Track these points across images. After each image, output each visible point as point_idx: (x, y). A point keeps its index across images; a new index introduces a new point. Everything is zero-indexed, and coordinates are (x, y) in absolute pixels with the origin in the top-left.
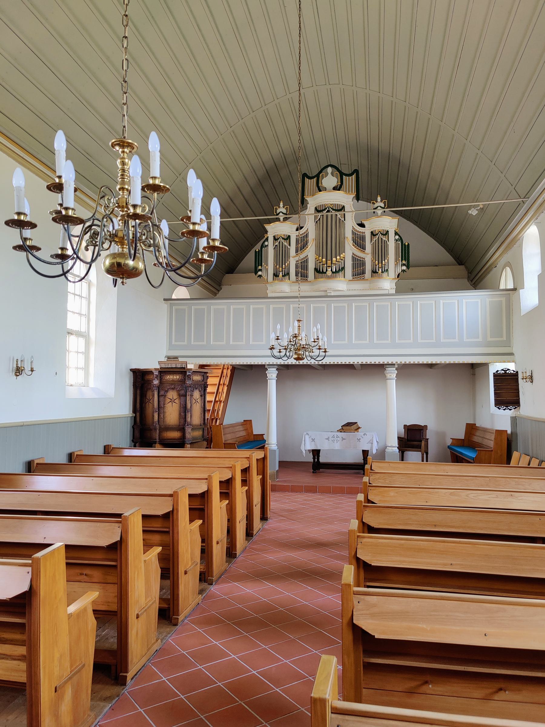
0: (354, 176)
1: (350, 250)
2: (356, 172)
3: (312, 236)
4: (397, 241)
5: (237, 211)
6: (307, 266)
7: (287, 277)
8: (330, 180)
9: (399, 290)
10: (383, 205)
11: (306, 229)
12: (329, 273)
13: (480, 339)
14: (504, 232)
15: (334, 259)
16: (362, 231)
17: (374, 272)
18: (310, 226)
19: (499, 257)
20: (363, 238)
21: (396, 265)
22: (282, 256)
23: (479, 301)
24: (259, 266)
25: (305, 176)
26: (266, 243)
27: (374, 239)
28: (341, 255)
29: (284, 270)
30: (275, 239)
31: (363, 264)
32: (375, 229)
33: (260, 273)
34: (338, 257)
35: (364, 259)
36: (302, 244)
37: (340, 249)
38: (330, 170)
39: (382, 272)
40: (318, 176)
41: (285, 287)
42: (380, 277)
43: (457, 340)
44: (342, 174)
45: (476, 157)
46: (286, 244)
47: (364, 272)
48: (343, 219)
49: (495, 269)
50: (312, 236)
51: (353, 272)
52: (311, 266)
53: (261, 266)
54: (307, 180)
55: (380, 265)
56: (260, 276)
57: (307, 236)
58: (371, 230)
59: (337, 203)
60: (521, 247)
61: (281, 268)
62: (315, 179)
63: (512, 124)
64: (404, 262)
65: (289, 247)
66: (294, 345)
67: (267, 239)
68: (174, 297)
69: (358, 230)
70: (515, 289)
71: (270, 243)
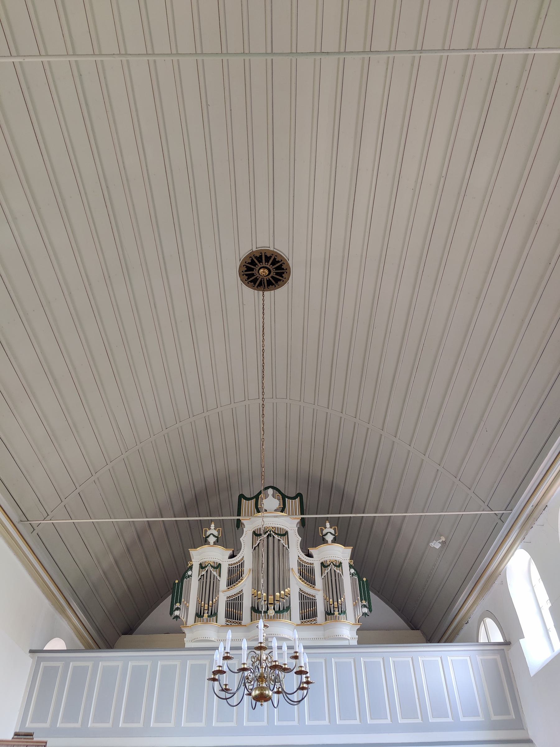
0: (298, 500)
1: (296, 585)
2: (299, 495)
3: (248, 566)
4: (353, 575)
5: (153, 541)
6: (241, 605)
7: (215, 618)
8: (271, 502)
9: (363, 641)
10: (333, 532)
11: (241, 557)
12: (271, 612)
13: (481, 718)
14: (479, 571)
15: (278, 594)
16: (309, 562)
17: (329, 613)
18: (246, 553)
19: (472, 605)
20: (312, 571)
21: (355, 606)
22: (209, 589)
23: (468, 658)
24: (176, 603)
25: (242, 497)
26: (189, 573)
27: (326, 572)
28: (286, 590)
29: (210, 608)
30: (202, 567)
31: (314, 604)
32: (325, 559)
33: (177, 613)
34: (282, 592)
35: (314, 596)
36: (235, 576)
37: (285, 584)
38: (270, 491)
39: (339, 614)
40: (257, 497)
41: (209, 632)
42: (336, 619)
43: (450, 720)
44: (284, 497)
45: (436, 475)
46: (215, 573)
47: (315, 615)
48: (287, 546)
49: (466, 627)
50: (248, 566)
51: (301, 614)
52: (247, 604)
53: (180, 603)
54: (243, 501)
55: (336, 603)
56: (177, 617)
57: (242, 565)
58: (321, 561)
59: (279, 526)
60: (504, 584)
61: (206, 606)
62: (253, 501)
63: (482, 423)
64: (364, 603)
65: (218, 578)
66: (253, 673)
67: (191, 568)
68: (46, 648)
69: (305, 560)
70: (507, 643)
71: (195, 573)
